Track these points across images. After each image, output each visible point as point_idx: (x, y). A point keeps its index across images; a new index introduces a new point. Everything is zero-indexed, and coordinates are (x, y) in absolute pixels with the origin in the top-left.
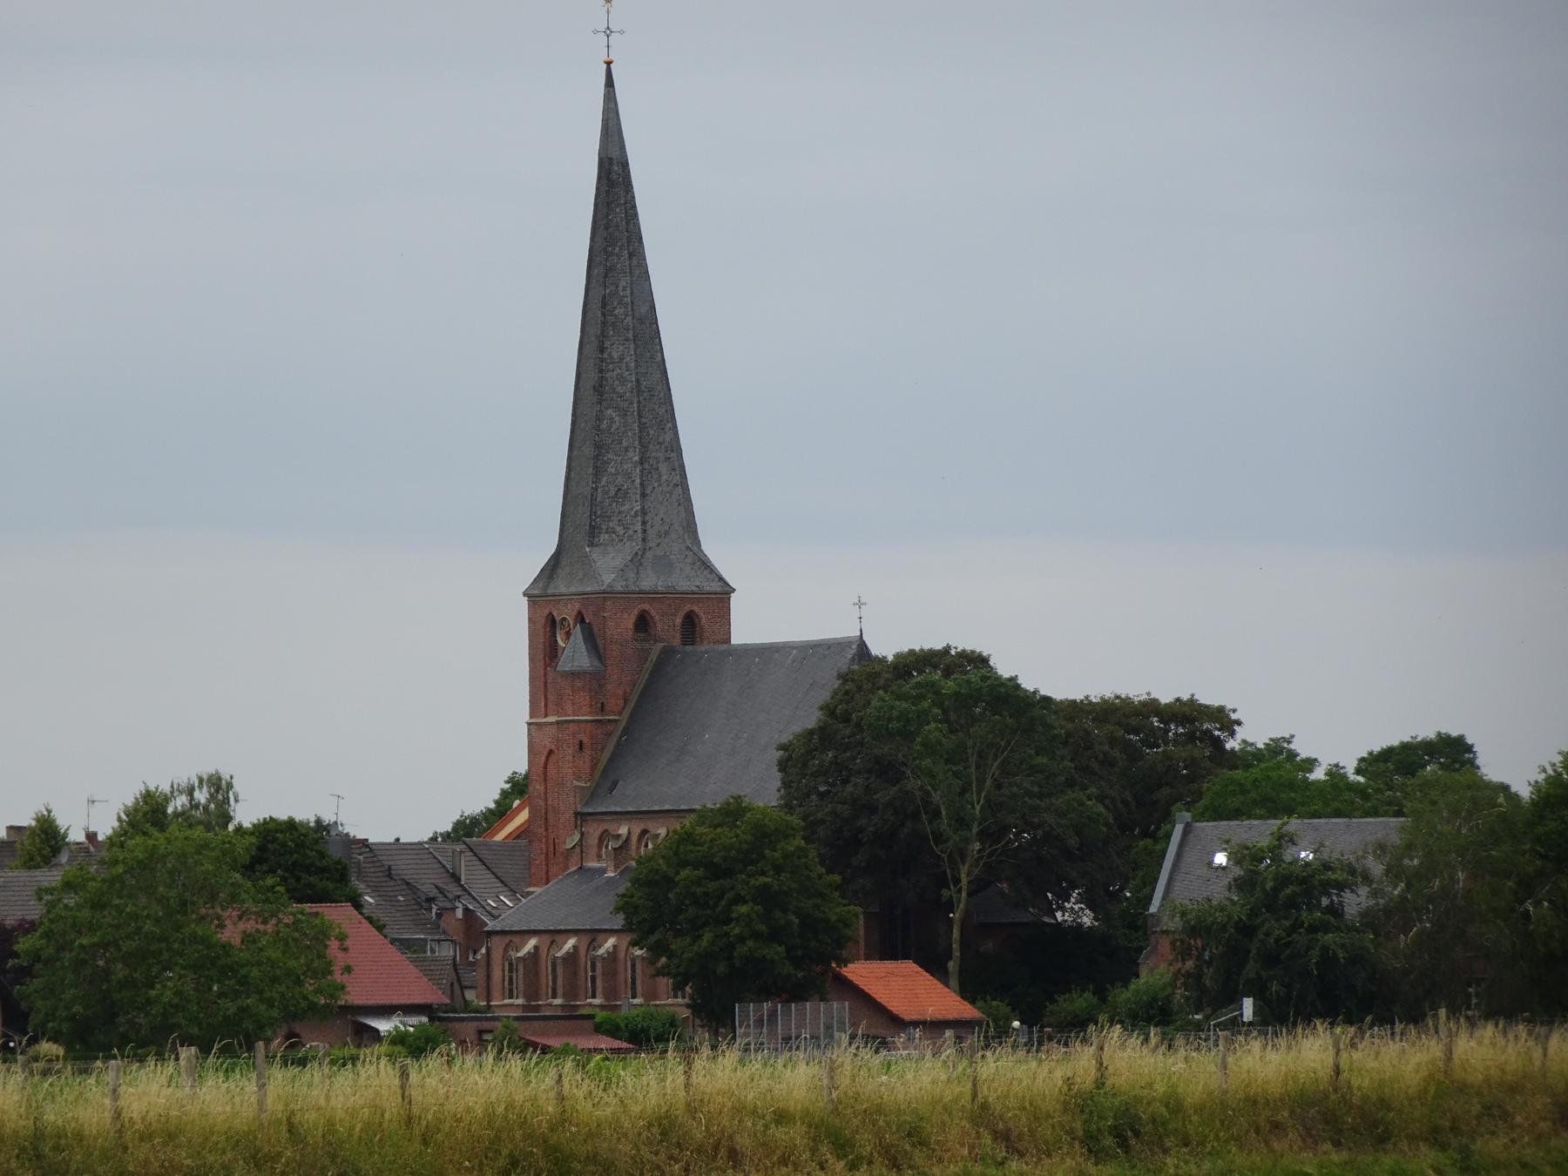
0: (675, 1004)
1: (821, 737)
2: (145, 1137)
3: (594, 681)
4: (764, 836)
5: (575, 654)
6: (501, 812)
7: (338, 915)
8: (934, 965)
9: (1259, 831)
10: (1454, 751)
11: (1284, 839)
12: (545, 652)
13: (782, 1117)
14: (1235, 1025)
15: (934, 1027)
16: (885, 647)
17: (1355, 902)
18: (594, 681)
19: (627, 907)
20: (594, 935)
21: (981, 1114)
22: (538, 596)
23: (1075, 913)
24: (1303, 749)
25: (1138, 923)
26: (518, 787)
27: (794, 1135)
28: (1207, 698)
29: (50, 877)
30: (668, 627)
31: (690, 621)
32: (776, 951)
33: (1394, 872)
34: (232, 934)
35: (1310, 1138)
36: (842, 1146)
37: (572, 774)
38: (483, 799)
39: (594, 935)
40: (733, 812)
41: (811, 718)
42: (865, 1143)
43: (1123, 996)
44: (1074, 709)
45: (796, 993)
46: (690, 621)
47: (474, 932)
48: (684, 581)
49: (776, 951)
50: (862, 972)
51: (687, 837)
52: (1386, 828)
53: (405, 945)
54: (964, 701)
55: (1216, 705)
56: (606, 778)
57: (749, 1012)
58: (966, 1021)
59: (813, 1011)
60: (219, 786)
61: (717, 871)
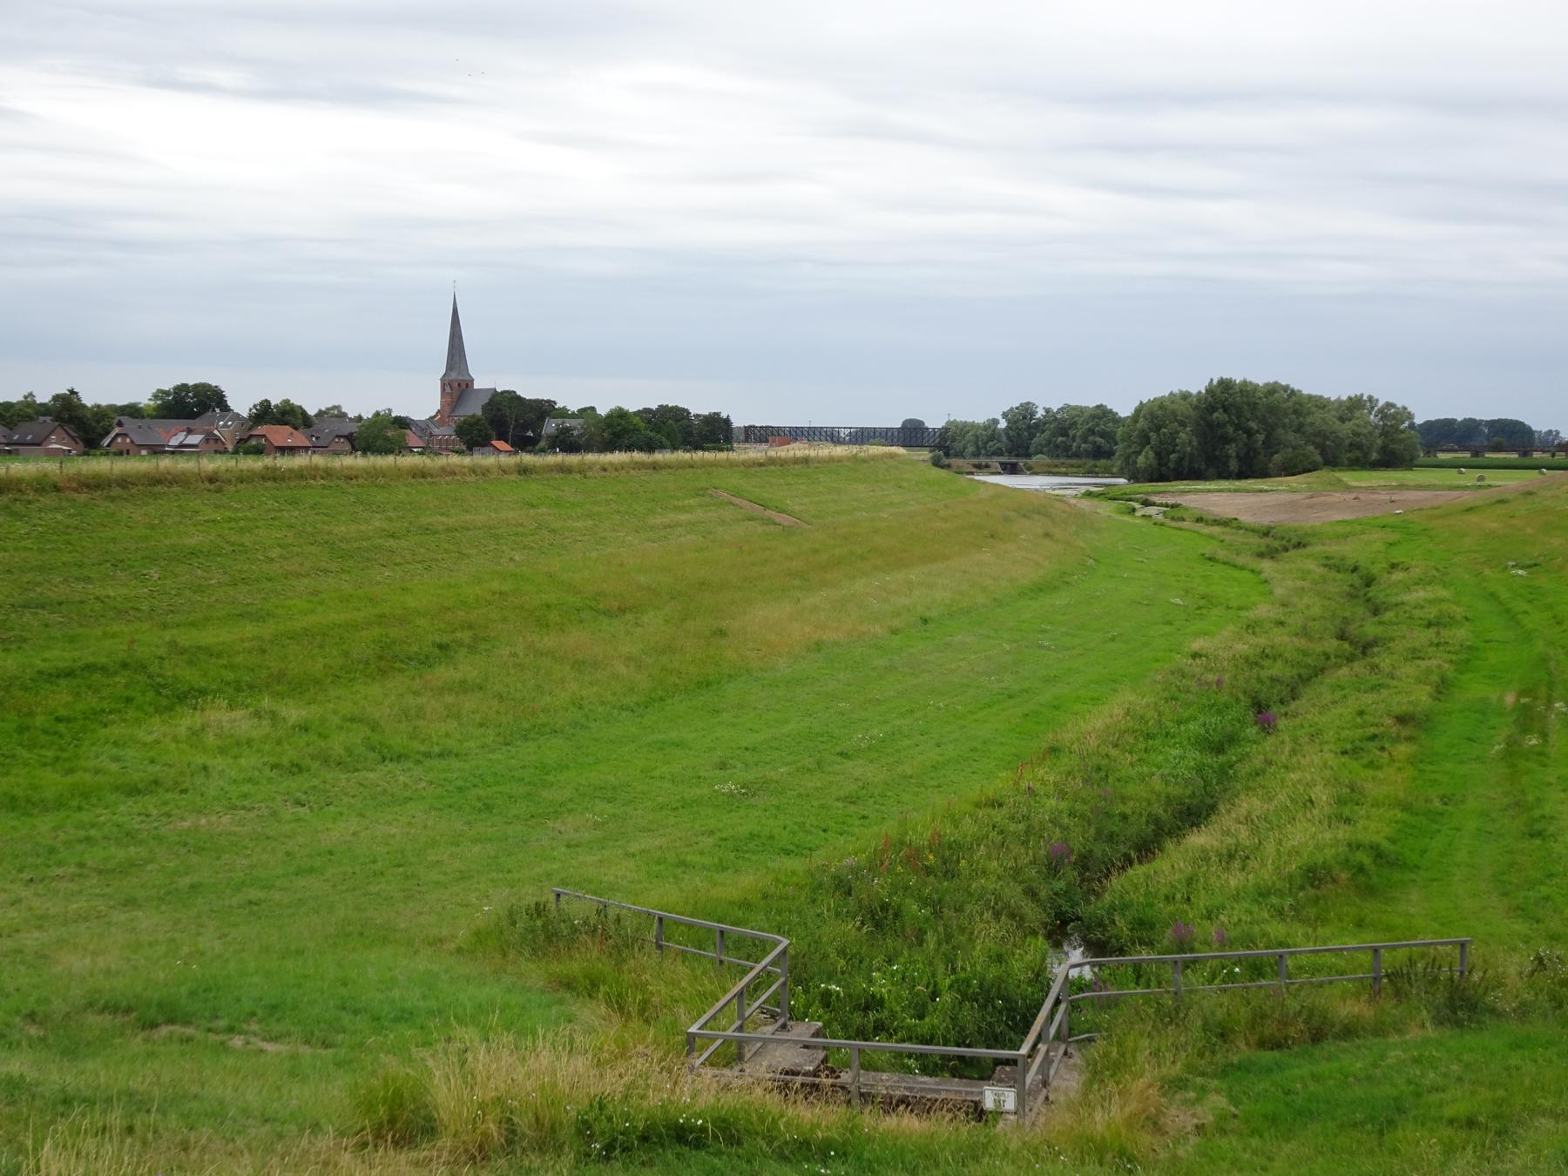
0: (464, 448)
1: (489, 403)
2: (347, 468)
3: (451, 394)
4: (479, 420)
5: (448, 389)
6: (573, 416)
7: (408, 431)
8: (507, 442)
9: (560, 421)
10: (593, 409)
11: (563, 423)
12: (443, 390)
13: (464, 467)
14: (555, 452)
15: (506, 452)
16: (499, 390)
17: (575, 433)
18: (451, 394)
19: (456, 431)
20: (450, 436)
21: (500, 467)
22: (441, 380)
23: (530, 434)
24: (568, 408)
25: (540, 435)
26: (439, 411)
27: (466, 470)
28: (552, 399)
29: (359, 424)
30: (464, 386)
31: (467, 385)
32: (480, 439)
33: (582, 428)
34: (389, 434)
35: (558, 472)
36: (474, 472)
37: (448, 409)
38: (433, 414)
39: (450, 436)
40: (474, 416)
41: (487, 401)
42: (479, 471)
43: (537, 447)
44: (530, 400)
45: (483, 446)
46: (467, 385)
47: (431, 435)
48: (466, 378)
49: (480, 439)
50: (493, 442)
51: (465, 420)
52: (581, 421)
53: (420, 437)
54: (512, 398)
55: (1092, 404)
56: (453, 410)
57: (475, 448)
58: (1387, 467)
59: (486, 449)
60: (390, 410)
61: (471, 425)
